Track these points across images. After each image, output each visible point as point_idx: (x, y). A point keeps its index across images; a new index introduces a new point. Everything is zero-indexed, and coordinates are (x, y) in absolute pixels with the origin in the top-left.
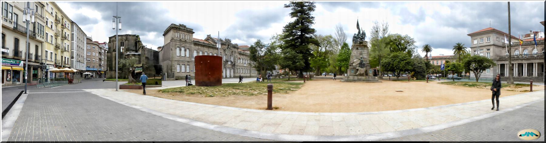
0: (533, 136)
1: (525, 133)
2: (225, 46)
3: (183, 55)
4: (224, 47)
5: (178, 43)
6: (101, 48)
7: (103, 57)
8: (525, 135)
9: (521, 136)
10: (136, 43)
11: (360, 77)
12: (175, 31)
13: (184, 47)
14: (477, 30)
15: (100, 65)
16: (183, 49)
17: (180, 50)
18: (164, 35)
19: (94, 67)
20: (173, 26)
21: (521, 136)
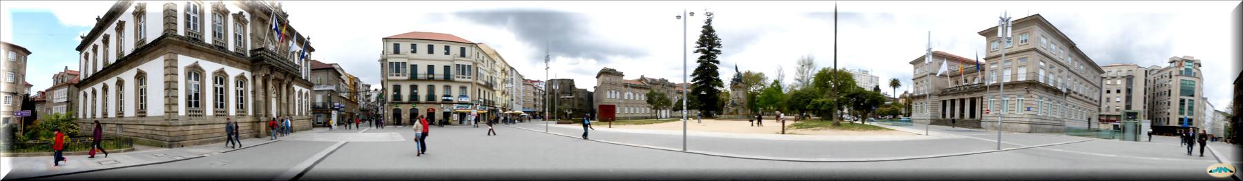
6: (535, 88)
7: (537, 97)
8: (1216, 171)
10: (571, 87)
11: (730, 116)
14: (999, 58)
15: (535, 106)
16: (613, 92)
17: (611, 92)
18: (597, 77)
19: (529, 108)
21: (1211, 172)
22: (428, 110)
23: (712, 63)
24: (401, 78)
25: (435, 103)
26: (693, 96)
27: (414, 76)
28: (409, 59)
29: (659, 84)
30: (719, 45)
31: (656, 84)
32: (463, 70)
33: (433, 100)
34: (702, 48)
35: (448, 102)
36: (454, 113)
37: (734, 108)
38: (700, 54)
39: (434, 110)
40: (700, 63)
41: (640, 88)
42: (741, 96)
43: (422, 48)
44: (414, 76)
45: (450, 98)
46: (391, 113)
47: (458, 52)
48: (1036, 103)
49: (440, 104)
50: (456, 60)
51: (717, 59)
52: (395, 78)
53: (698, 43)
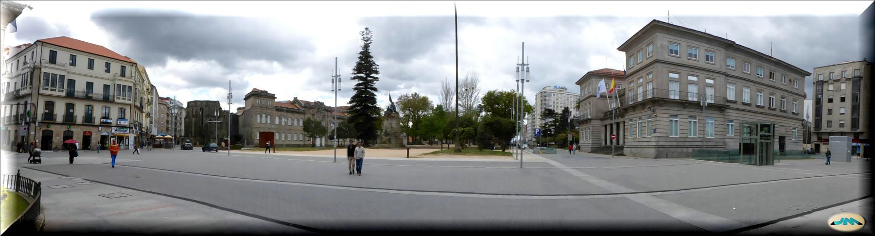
0: (853, 224)
1: (840, 220)
2: (314, 110)
3: (264, 121)
4: (312, 111)
5: (259, 110)
8: (839, 223)
9: (833, 224)
11: (383, 145)
12: (256, 97)
13: (265, 113)
16: (264, 116)
20: (254, 93)
21: (833, 224)
22: (85, 132)
23: (370, 91)
24: (57, 93)
25: (93, 126)
26: (349, 125)
27: (71, 95)
28: (68, 73)
29: (313, 108)
30: (377, 72)
31: (311, 108)
32: (122, 89)
33: (91, 122)
34: (359, 75)
35: (108, 125)
36: (112, 137)
37: (387, 138)
38: (356, 82)
39: (91, 133)
40: (356, 91)
41: (293, 112)
42: (394, 126)
43: (82, 61)
44: (71, 95)
45: (109, 121)
46: (40, 135)
47: (119, 72)
48: (667, 123)
49: (98, 126)
50: (118, 80)
51: (375, 86)
52: (49, 92)
53: (354, 69)
